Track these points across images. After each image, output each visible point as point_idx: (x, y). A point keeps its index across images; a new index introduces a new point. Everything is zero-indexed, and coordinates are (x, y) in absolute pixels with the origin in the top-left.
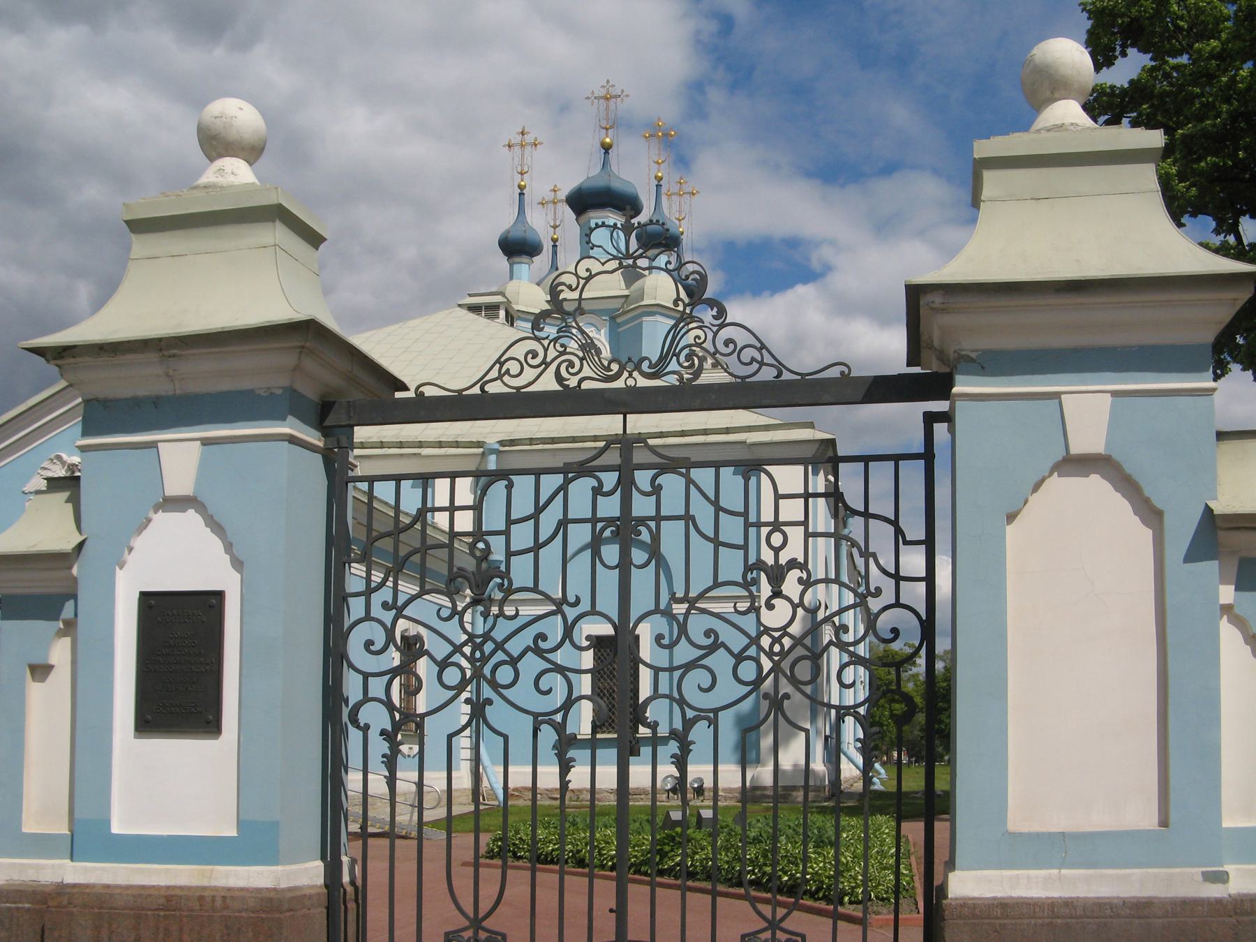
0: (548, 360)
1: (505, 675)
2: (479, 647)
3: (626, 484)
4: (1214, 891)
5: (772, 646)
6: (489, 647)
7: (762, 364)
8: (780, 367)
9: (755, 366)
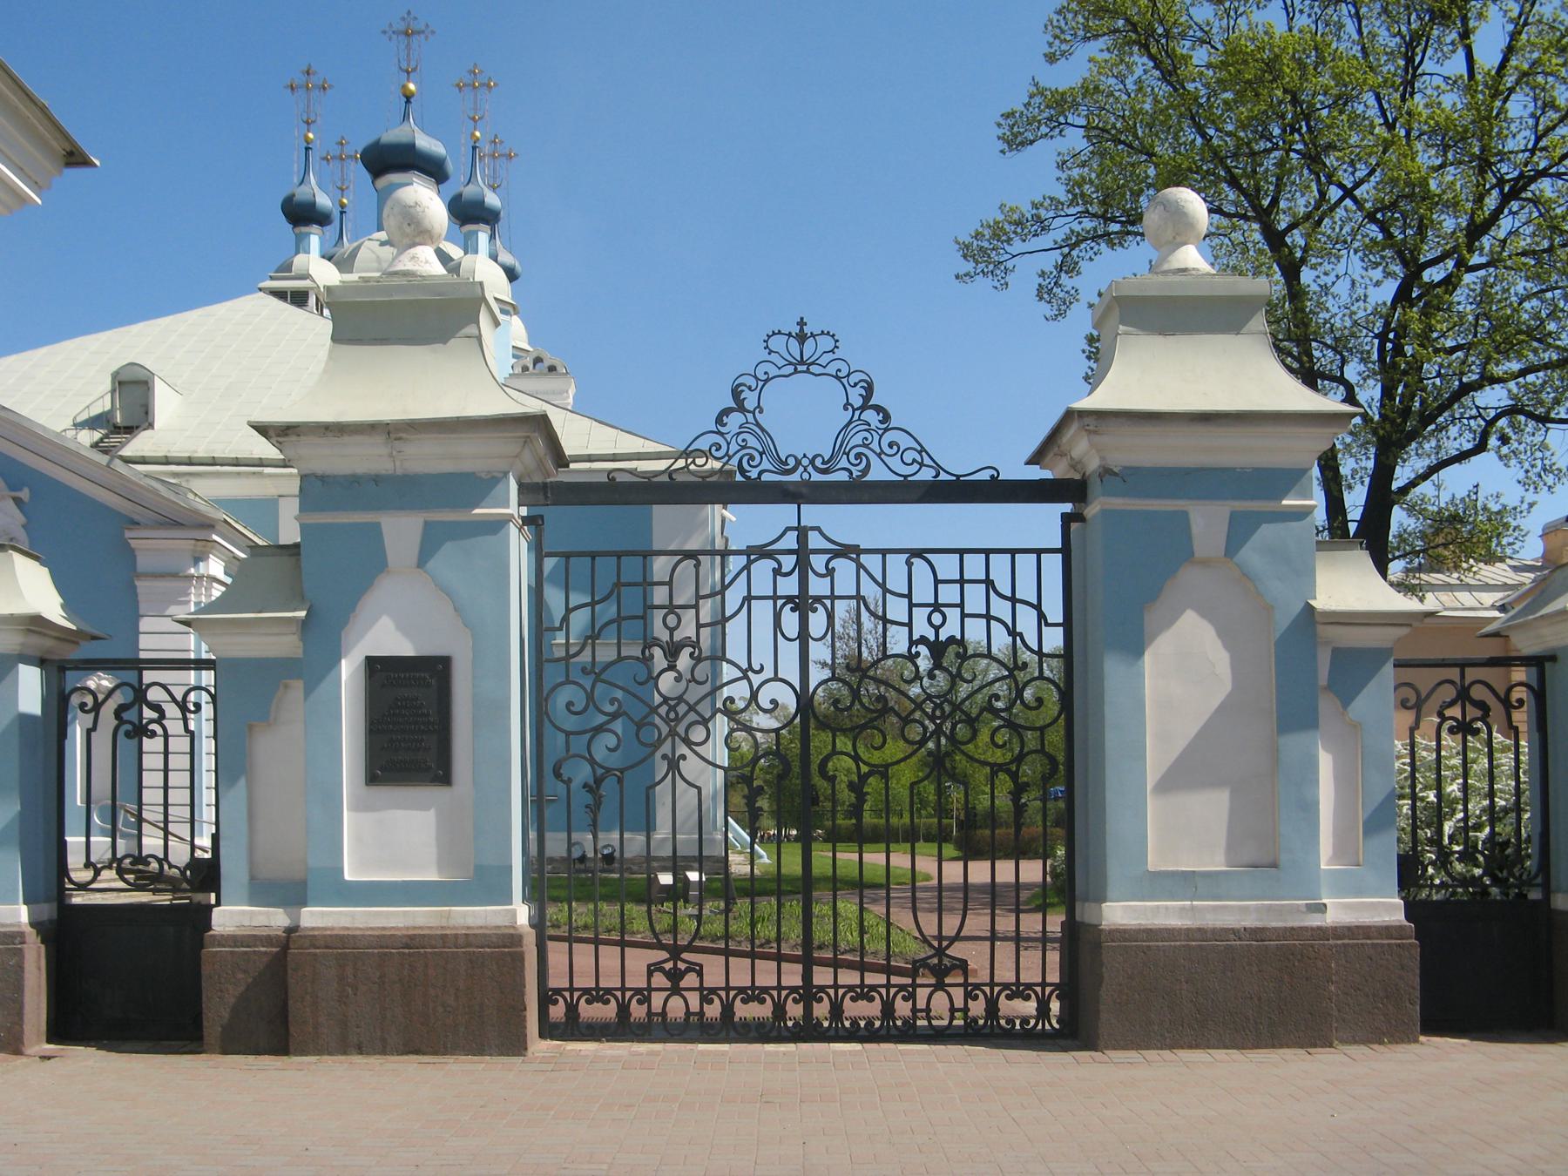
0: (731, 453)
1: (698, 734)
2: (672, 708)
3: (803, 566)
4: (1314, 921)
5: (934, 711)
6: (682, 709)
7: (922, 464)
8: (938, 468)
9: (916, 467)
